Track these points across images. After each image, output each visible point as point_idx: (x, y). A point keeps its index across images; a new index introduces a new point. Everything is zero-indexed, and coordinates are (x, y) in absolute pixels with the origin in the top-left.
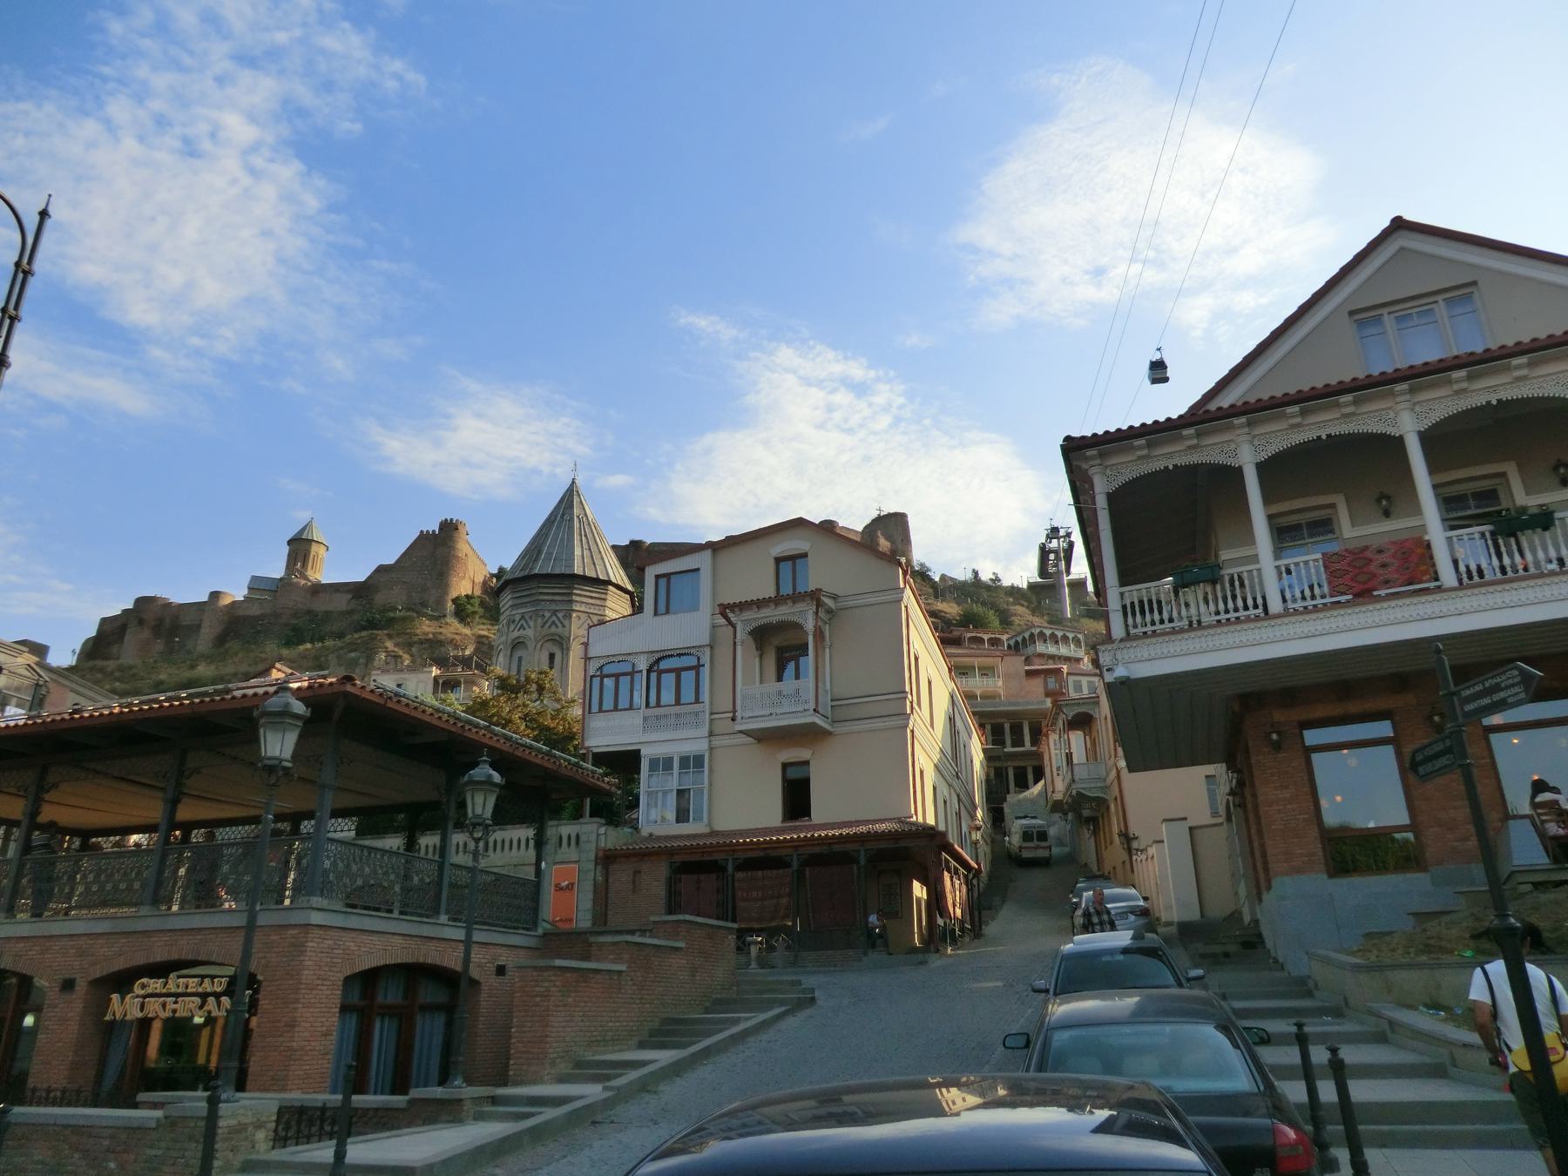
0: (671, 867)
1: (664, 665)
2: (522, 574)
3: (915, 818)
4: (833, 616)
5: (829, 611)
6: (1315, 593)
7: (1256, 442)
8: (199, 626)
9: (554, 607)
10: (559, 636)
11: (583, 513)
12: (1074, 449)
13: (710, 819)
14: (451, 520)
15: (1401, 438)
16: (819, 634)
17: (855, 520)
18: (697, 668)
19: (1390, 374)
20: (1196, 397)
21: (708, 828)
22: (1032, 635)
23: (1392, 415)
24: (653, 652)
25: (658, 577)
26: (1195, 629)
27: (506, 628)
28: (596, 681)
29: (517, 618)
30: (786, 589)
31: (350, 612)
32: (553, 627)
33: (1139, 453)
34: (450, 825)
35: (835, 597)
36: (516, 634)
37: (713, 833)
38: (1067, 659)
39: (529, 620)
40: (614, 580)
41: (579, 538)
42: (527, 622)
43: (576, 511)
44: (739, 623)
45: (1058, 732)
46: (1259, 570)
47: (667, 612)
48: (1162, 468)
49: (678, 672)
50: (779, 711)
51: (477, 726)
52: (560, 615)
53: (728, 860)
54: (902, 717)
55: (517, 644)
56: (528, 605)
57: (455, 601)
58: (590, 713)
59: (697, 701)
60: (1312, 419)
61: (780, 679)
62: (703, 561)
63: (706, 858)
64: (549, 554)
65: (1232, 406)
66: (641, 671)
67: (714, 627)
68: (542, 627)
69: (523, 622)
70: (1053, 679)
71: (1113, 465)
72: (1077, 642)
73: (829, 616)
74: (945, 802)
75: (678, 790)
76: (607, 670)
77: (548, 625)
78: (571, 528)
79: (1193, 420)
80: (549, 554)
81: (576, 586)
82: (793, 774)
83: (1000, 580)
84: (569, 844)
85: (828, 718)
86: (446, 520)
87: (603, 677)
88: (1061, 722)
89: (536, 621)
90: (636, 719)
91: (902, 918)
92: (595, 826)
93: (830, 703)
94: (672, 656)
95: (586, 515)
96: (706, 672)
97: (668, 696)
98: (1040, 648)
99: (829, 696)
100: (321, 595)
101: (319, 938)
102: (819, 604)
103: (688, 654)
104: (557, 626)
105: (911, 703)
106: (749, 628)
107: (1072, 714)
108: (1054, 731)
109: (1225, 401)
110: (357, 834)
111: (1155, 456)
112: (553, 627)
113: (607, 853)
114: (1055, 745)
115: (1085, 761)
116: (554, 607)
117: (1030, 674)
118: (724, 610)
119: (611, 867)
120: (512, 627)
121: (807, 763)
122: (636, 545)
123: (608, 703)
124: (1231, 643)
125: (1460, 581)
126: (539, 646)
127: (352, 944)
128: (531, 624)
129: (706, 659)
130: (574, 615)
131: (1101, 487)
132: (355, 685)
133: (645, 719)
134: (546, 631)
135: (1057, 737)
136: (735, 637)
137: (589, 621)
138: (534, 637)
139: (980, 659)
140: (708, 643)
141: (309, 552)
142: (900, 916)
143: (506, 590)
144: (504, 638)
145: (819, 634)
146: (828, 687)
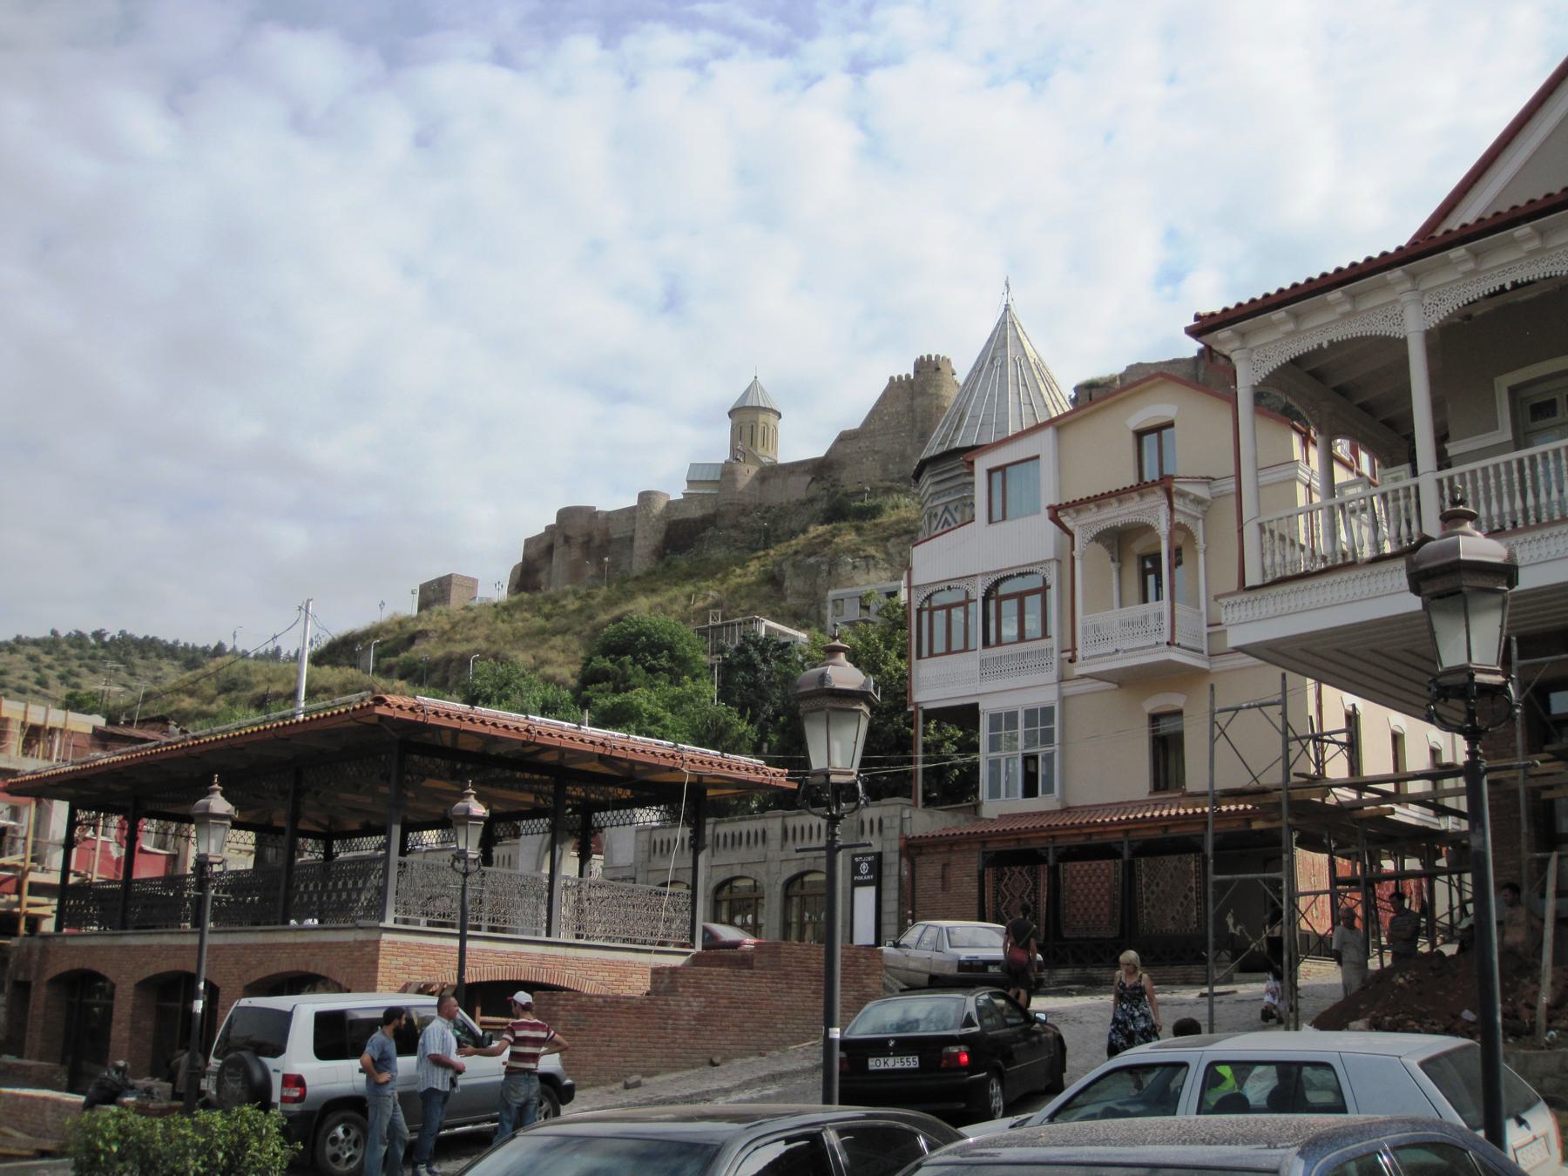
0: (984, 858)
1: (1004, 589)
4: (1209, 507)
7: (1427, 301)
8: (632, 539)
11: (1021, 351)
14: (929, 357)
18: (1043, 590)
23: (1399, 308)
24: (987, 574)
25: (990, 472)
26: (1533, 528)
29: (940, 510)
31: (811, 501)
33: (1340, 310)
37: (1067, 810)
39: (953, 512)
46: (1417, 488)
47: (1004, 518)
49: (1020, 597)
53: (1047, 848)
56: (952, 491)
58: (919, 656)
60: (1492, 262)
63: (1023, 846)
64: (974, 417)
65: (1480, 220)
66: (976, 600)
69: (947, 515)
71: (1432, 289)
73: (1200, 508)
75: (974, 708)
76: (938, 600)
78: (1004, 375)
82: (1166, 727)
84: (872, 832)
85: (1202, 652)
86: (922, 358)
90: (968, 664)
92: (899, 807)
93: (1205, 630)
94: (1011, 577)
95: (1025, 355)
96: (1053, 594)
97: (1010, 631)
99: (1205, 619)
100: (772, 481)
106: (1090, 535)
109: (1469, 214)
111: (1306, 331)
113: (909, 842)
120: (934, 524)
123: (939, 646)
127: (434, 961)
129: (1052, 580)
133: (983, 662)
136: (1073, 548)
140: (1052, 557)
141: (756, 423)
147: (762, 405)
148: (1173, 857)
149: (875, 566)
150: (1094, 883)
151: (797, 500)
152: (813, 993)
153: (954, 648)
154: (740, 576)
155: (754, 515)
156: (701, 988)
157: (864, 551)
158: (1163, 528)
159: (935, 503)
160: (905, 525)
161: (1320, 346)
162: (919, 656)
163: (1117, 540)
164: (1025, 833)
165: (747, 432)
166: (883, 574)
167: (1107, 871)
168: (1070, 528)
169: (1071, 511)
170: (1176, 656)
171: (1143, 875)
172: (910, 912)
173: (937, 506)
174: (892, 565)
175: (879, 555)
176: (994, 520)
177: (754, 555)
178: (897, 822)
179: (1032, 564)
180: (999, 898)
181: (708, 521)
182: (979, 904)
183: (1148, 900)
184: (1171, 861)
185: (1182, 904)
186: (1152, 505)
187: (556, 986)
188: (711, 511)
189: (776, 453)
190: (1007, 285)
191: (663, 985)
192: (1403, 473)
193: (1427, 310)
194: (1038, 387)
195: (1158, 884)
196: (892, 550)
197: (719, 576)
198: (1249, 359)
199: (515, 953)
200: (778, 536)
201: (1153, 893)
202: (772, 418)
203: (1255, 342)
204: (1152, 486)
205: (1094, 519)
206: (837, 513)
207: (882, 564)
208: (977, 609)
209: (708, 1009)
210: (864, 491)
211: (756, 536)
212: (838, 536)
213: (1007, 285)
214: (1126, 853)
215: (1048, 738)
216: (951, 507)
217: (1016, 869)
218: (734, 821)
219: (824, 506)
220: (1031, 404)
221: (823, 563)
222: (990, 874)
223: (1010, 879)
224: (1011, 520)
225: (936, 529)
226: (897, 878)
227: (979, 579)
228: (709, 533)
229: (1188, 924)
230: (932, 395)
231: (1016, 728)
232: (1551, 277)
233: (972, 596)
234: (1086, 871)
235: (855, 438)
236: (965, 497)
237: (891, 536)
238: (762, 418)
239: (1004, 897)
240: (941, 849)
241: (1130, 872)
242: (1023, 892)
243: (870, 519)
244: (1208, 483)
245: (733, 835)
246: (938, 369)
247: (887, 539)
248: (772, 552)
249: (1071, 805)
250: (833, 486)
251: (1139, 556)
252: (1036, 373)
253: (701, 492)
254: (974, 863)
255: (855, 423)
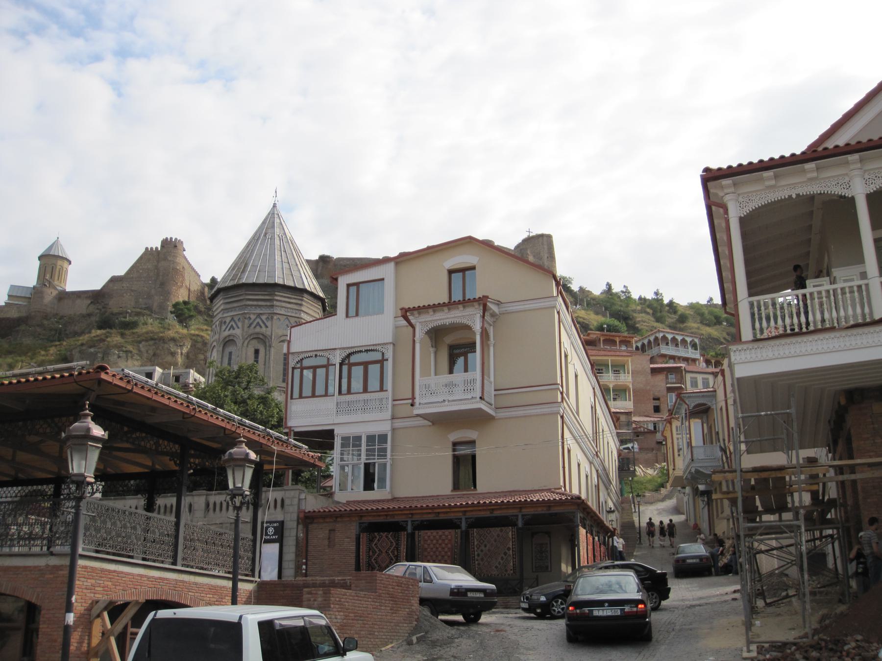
0: (360, 527)
1: (353, 359)
2: (231, 283)
3: (563, 489)
4: (497, 319)
5: (493, 315)
6: (786, 323)
9: (258, 311)
10: (263, 335)
12: (710, 177)
13: (391, 487)
14: (171, 238)
15: (853, 198)
16: (485, 334)
17: (510, 240)
18: (382, 362)
19: (864, 143)
20: (814, 137)
21: (390, 495)
22: (656, 339)
24: (344, 348)
25: (349, 286)
27: (218, 328)
28: (297, 372)
30: (457, 296)
31: (89, 315)
32: (258, 327)
34: (184, 489)
35: (499, 303)
36: (227, 333)
37: (394, 499)
38: (686, 360)
40: (309, 289)
41: (279, 254)
42: (235, 323)
43: (277, 231)
44: (418, 324)
45: (680, 419)
46: (867, 285)
47: (357, 315)
48: (787, 197)
49: (366, 365)
50: (451, 398)
51: (205, 408)
52: (264, 317)
53: (407, 521)
54: (555, 405)
55: (228, 342)
56: (237, 309)
57: (176, 305)
58: (292, 398)
59: (382, 389)
60: (783, 182)
61: (451, 371)
62: (388, 270)
64: (254, 266)
65: (847, 145)
66: (335, 365)
67: (397, 327)
68: (249, 327)
70: (673, 376)
72: (694, 346)
73: (492, 320)
74: (587, 476)
76: (306, 363)
77: (253, 326)
78: (273, 244)
79: (815, 155)
80: (254, 266)
81: (276, 293)
82: (464, 451)
83: (629, 293)
86: (167, 238)
87: (302, 369)
88: (684, 412)
89: (243, 322)
90: (329, 404)
91: (551, 571)
92: (297, 492)
93: (493, 393)
94: (361, 351)
95: (285, 234)
97: (357, 385)
98: (665, 350)
99: (493, 385)
101: (84, 578)
102: (485, 308)
103: (374, 350)
104: (261, 327)
105: (562, 393)
106: (426, 329)
107: (693, 405)
108: (677, 419)
109: (841, 140)
110: (103, 496)
112: (258, 327)
114: (677, 431)
115: (702, 444)
116: (258, 311)
117: (654, 371)
118: (405, 313)
119: (310, 526)
120: (224, 327)
121: (472, 443)
122: (324, 259)
123: (307, 391)
124: (743, 359)
125: (755, 335)
126: (245, 344)
127: (110, 583)
128: (240, 324)
129: (389, 355)
130: (275, 317)
131: (735, 214)
132: (107, 373)
134: (251, 331)
135: (679, 424)
136: (414, 336)
137: (287, 322)
138: (242, 335)
139: (614, 358)
140: (391, 341)
141: (56, 265)
142: (549, 569)
143: (219, 296)
144: (217, 337)
145: (485, 334)
146: (492, 379)
147: (60, 255)
148: (497, 528)
149: (132, 357)
150: (440, 544)
151: (81, 314)
152: (391, 610)
153: (317, 394)
154: (43, 355)
155: (52, 320)
156: (342, 605)
157: (126, 347)
158: (477, 327)
159: (225, 315)
160: (151, 335)
161: (790, 197)
162: (292, 398)
163: (436, 334)
164: (393, 511)
165: (49, 269)
166: (136, 363)
167: (449, 537)
168: (413, 323)
169: (416, 312)
170: (483, 406)
171: (475, 540)
172: (304, 561)
173: (226, 317)
174: (141, 358)
175: (135, 351)
176: (350, 315)
177: (52, 344)
178: (296, 501)
179: (375, 345)
180: (371, 553)
181: (20, 321)
182: (356, 557)
183: (478, 555)
184: (495, 531)
185: (502, 558)
186: (471, 313)
187: (183, 604)
188: (24, 314)
189: (65, 285)
190: (276, 192)
191: (316, 603)
192: (824, 283)
193: (867, 182)
194: (292, 253)
195: (485, 546)
196: (143, 349)
197: (30, 354)
198: (737, 200)
199: (160, 578)
200: (67, 334)
201: (482, 551)
202: (65, 264)
203: (870, 166)
204: (473, 302)
205: (431, 319)
206: (106, 323)
207: (136, 357)
208: (335, 372)
209: (345, 621)
210: (127, 313)
211: (53, 333)
212: (110, 337)
213: (276, 192)
214: (464, 526)
215: (383, 452)
216: (236, 319)
217: (384, 535)
218: (167, 497)
219: (97, 319)
220: (289, 263)
221: (99, 352)
222: (364, 537)
223: (379, 540)
224: (367, 314)
225: (225, 331)
226: (295, 538)
227: (338, 352)
228: (23, 327)
229: (506, 571)
230: (170, 261)
231: (386, 443)
232: (821, 193)
233: (333, 361)
234: (434, 537)
235: (120, 281)
236: (245, 313)
237: (143, 340)
238: (60, 262)
239: (374, 552)
240: (328, 520)
241: (466, 536)
242: (389, 549)
243: (129, 330)
244: (498, 304)
245: (166, 506)
246: (176, 246)
247: (140, 342)
248: (65, 343)
249: (396, 496)
250: (104, 308)
251: (448, 345)
252: (291, 245)
253: (16, 303)
254: (353, 529)
255: (121, 271)
